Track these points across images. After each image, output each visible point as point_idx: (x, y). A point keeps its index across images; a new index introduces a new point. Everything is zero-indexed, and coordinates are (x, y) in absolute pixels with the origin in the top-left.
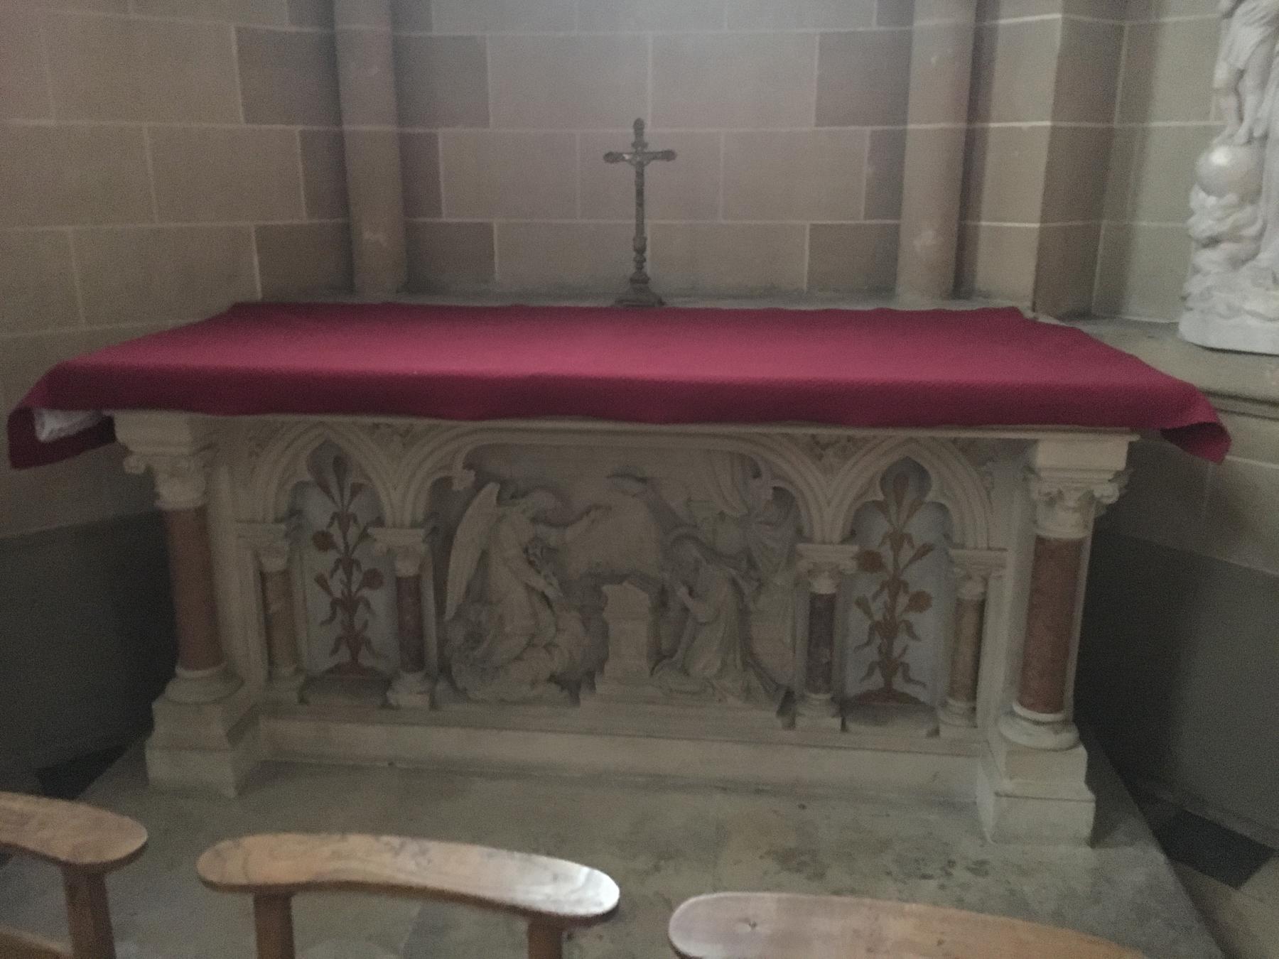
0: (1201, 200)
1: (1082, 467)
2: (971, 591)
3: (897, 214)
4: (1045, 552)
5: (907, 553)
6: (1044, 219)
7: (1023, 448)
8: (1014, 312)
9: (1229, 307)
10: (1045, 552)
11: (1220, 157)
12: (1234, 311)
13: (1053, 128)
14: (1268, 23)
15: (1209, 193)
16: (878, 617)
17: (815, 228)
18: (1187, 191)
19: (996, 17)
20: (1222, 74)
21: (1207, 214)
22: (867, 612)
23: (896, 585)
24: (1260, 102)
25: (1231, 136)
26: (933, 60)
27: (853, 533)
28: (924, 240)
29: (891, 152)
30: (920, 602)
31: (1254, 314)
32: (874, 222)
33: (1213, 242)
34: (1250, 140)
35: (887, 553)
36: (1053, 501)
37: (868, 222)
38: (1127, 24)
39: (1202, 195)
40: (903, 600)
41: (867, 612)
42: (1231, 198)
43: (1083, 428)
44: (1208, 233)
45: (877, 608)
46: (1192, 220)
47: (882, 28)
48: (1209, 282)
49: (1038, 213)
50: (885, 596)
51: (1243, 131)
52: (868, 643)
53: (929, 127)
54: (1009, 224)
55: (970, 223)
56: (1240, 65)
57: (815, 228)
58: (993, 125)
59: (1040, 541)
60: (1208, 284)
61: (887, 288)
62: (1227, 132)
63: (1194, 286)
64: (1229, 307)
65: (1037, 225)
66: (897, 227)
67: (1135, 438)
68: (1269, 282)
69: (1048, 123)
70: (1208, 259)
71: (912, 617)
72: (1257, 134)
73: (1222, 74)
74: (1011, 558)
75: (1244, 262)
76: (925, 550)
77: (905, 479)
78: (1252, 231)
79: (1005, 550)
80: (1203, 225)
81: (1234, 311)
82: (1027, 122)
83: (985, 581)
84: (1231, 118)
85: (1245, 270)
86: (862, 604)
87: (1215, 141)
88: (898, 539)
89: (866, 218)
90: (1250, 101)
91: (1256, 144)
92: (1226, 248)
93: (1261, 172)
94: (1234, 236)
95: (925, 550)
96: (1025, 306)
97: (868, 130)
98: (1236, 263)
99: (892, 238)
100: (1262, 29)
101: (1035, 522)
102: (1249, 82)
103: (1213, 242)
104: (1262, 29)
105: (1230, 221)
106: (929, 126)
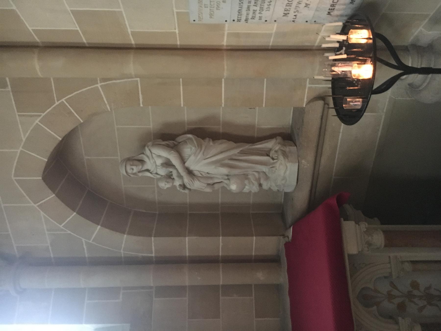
0: (247, 189)
1: (356, 236)
2: (408, 267)
3: (250, 285)
4: (391, 242)
5: (395, 292)
6: (252, 236)
7: (349, 255)
8: (287, 245)
9: (283, 180)
10: (391, 242)
11: (234, 187)
12: (284, 178)
13: (222, 236)
14: (193, 179)
15: (244, 188)
16: (425, 303)
17: (257, 317)
18: (244, 193)
19: (186, 257)
20: (208, 190)
21: (251, 188)
22: (424, 307)
23: (410, 296)
24: (217, 178)
25: (227, 184)
26: (199, 278)
27: (391, 317)
28: (261, 276)
29: (228, 289)
30: (415, 285)
31: (285, 173)
32: (253, 293)
33: (260, 185)
34: (228, 179)
35: (397, 301)
36: (369, 244)
37: (253, 295)
38: (189, 212)
39: (245, 189)
40: (416, 292)
41: (424, 307)
42: (246, 182)
43: (266, 141)
44: (258, 188)
45: (421, 303)
46: (253, 191)
47: (187, 295)
48: (273, 185)
49: (250, 238)
50: (416, 300)
51: (226, 182)
52: (437, 306)
53: (221, 277)
54: (254, 246)
55: (253, 258)
56: (206, 185)
57: (257, 317)
58: (220, 254)
59: (385, 246)
60: (274, 185)
61: (278, 288)
62: (225, 186)
63: (275, 189)
64: (283, 180)
65: (254, 237)
66: (256, 285)
67: (342, 219)
68: (274, 169)
69: (221, 237)
70: (265, 186)
71: (422, 288)
72: (227, 178)
73: (208, 190)
74: (392, 255)
75: (266, 175)
76: (392, 284)
77: (367, 300)
78: (256, 174)
79: (389, 257)
80: (255, 189)
81: (284, 178)
82: (220, 244)
83: (403, 262)
84: (221, 185)
85: (269, 175)
86: (421, 309)
87: (228, 189)
88: (390, 297)
89: (131, 32)
90: (216, 181)
91: (229, 177)
92: (262, 182)
93: (237, 175)
94: (258, 180)
95: (392, 284)
96: (283, 241)
97: (221, 298)
98: (267, 178)
99: (260, 287)
100: (195, 181)
101: (378, 248)
102: (211, 182)
103: (260, 185)
104: (195, 181)
105: (254, 182)
106: (221, 277)
